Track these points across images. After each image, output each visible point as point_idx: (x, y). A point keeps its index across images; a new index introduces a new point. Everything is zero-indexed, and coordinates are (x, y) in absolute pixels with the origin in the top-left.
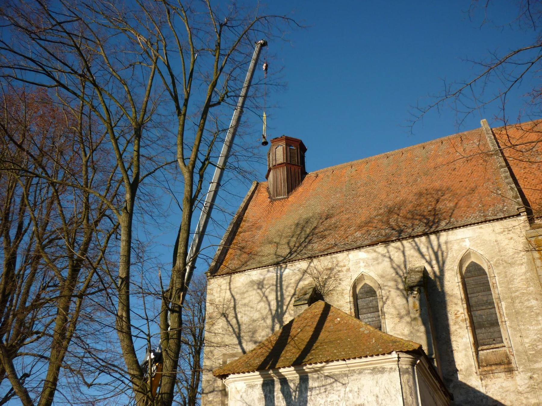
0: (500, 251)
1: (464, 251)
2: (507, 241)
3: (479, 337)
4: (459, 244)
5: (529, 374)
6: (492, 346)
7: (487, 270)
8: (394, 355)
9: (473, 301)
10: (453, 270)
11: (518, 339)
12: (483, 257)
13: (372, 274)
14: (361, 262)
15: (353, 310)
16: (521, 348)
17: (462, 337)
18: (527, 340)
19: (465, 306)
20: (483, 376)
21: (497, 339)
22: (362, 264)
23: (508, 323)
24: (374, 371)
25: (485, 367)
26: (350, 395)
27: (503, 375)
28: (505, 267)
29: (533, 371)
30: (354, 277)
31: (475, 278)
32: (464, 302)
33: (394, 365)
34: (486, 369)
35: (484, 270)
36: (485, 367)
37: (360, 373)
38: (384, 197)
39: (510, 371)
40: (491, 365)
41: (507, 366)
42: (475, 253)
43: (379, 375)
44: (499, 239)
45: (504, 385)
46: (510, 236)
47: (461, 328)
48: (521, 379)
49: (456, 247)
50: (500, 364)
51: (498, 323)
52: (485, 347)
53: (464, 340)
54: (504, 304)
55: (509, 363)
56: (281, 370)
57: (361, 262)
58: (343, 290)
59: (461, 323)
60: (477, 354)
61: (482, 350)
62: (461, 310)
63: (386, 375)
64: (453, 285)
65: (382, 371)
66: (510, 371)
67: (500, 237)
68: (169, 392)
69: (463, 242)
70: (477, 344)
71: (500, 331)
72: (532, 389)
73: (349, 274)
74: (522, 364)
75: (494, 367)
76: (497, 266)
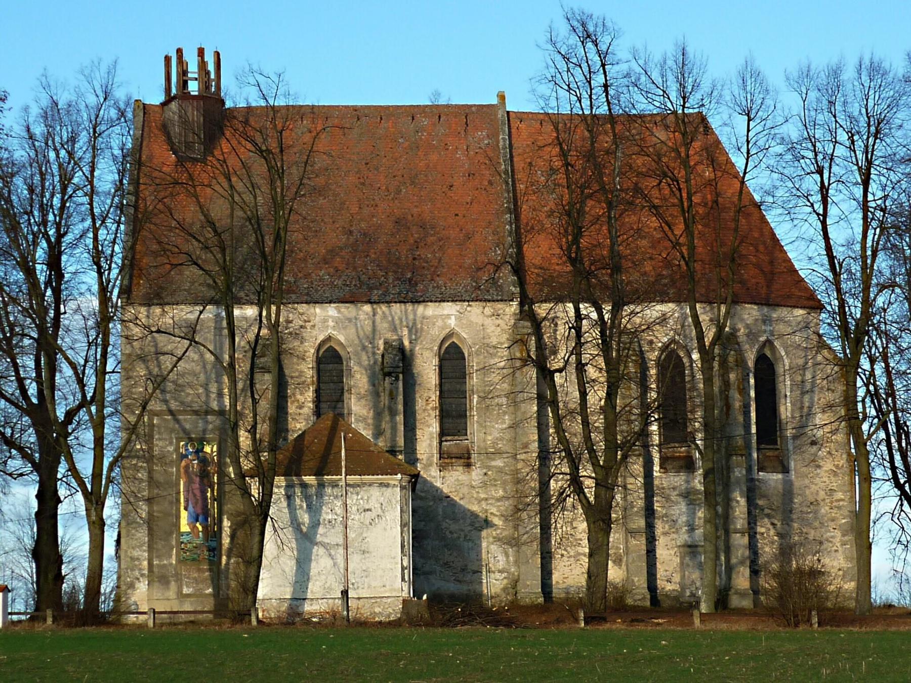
0: (484, 338)
1: (448, 330)
2: (493, 328)
3: (446, 426)
4: (443, 320)
5: (485, 471)
6: (456, 437)
7: (466, 355)
8: (399, 476)
9: (445, 388)
10: (432, 351)
11: (482, 435)
12: (466, 337)
13: (342, 338)
14: (330, 320)
15: (315, 379)
16: (482, 445)
17: (429, 426)
18: (490, 438)
19: (438, 393)
20: (442, 468)
21: (461, 431)
22: (331, 323)
23: (476, 418)
24: (381, 485)
25: (447, 459)
26: (361, 502)
27: (461, 468)
28: (485, 357)
29: (489, 468)
30: (321, 338)
31: (452, 359)
32: (438, 389)
33: (397, 483)
34: (446, 461)
35: (463, 354)
36: (447, 459)
37: (370, 485)
38: (354, 209)
39: (468, 465)
40: (452, 458)
41: (465, 459)
42: (458, 335)
43: (385, 489)
44: (486, 323)
45: (460, 478)
46: (498, 322)
47: (429, 415)
48: (476, 474)
49: (440, 323)
50: (461, 458)
51: (466, 416)
52: (449, 438)
53: (431, 429)
54: (475, 399)
55: (469, 458)
57: (330, 320)
58: (305, 352)
59: (431, 412)
60: (440, 445)
61: (446, 441)
62: (433, 398)
63: (390, 490)
64: (428, 369)
65: (387, 486)
66: (468, 465)
67: (488, 322)
68: (557, 593)
69: (445, 317)
70: (443, 434)
71: (466, 423)
72: (484, 485)
73: (314, 333)
74: (481, 460)
75: (454, 460)
76: (478, 355)
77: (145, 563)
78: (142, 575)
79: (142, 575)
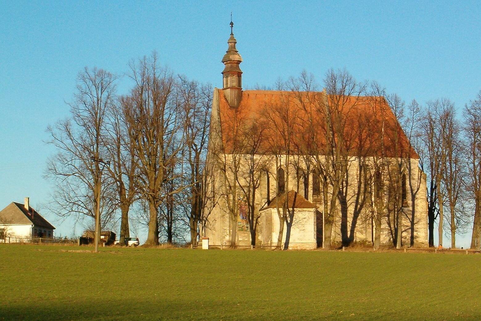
56: (289, 209)
77: (228, 231)
78: (227, 234)
79: (227, 234)
